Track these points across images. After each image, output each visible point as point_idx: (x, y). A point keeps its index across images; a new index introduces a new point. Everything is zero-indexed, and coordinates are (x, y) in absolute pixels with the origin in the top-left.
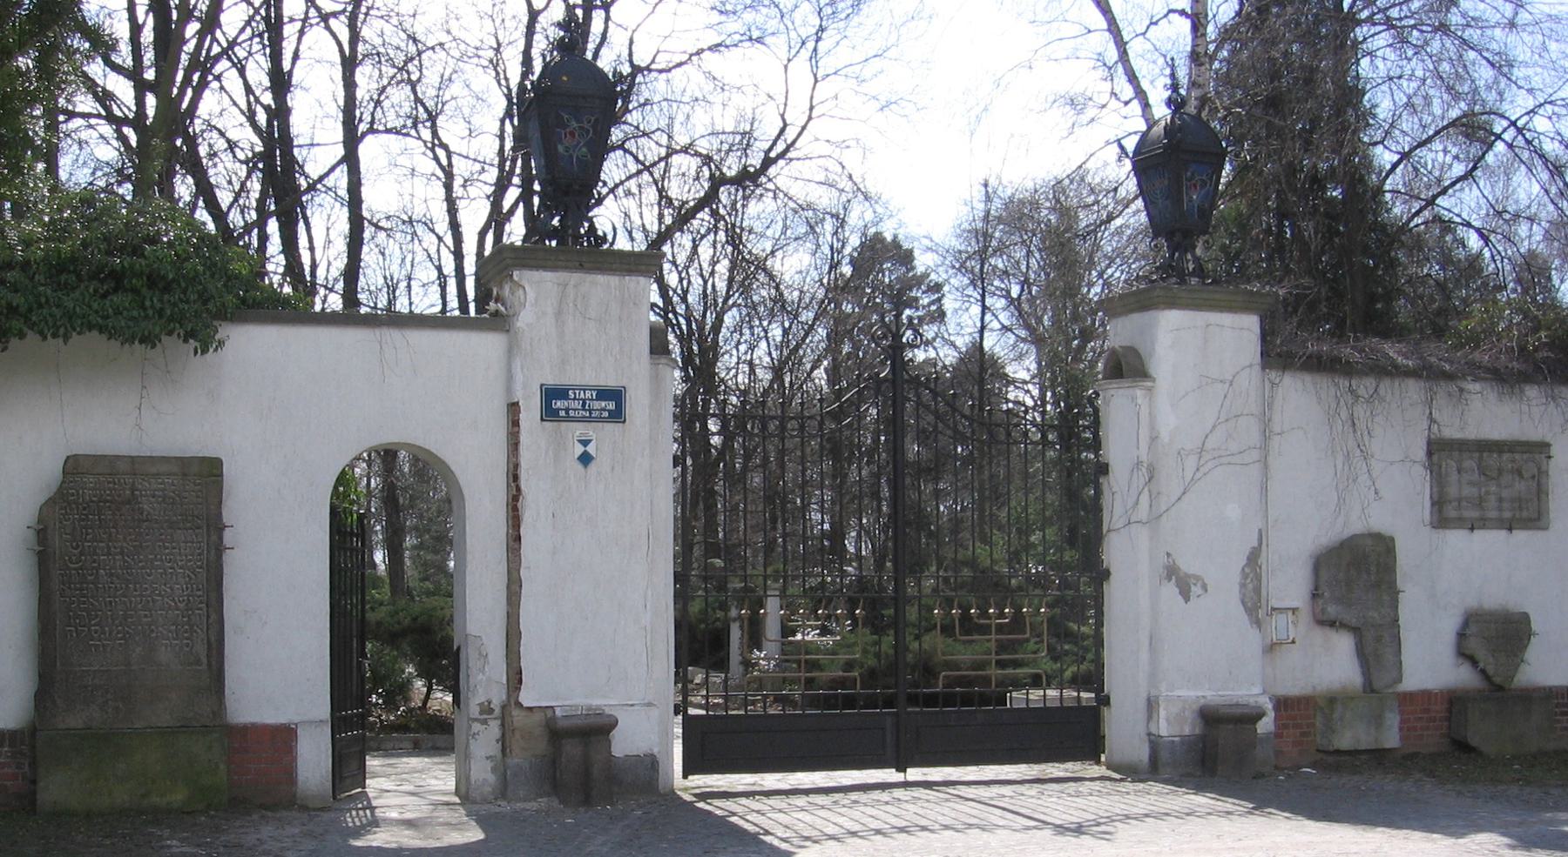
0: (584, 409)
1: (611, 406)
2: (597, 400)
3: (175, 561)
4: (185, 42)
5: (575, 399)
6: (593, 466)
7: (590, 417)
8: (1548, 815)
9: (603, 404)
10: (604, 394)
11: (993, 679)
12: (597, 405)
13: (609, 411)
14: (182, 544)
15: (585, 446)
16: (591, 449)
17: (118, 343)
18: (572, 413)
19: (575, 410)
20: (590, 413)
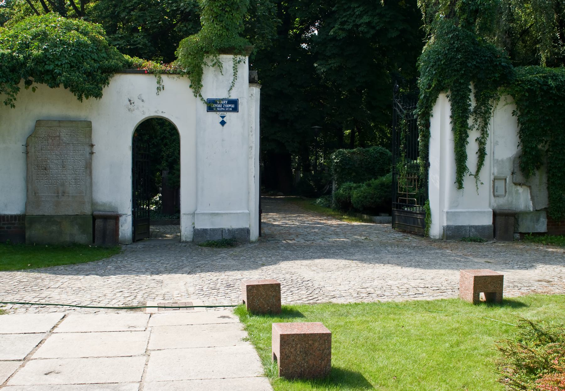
0: (223, 107)
1: (233, 106)
2: (227, 104)
3: (75, 157)
4: (405, 147)
5: (219, 104)
6: (225, 125)
7: (225, 110)
8: (279, 20)
9: (230, 105)
10: (231, 102)
11: (17, 217)
12: (228, 106)
13: (232, 108)
14: (77, 152)
15: (223, 120)
16: (225, 119)
17: (464, 177)
18: (218, 109)
19: (219, 108)
20: (225, 109)
